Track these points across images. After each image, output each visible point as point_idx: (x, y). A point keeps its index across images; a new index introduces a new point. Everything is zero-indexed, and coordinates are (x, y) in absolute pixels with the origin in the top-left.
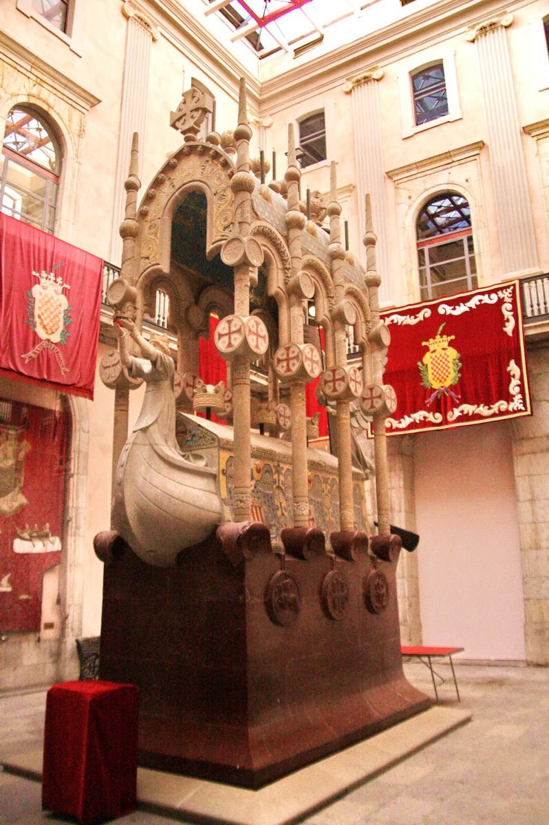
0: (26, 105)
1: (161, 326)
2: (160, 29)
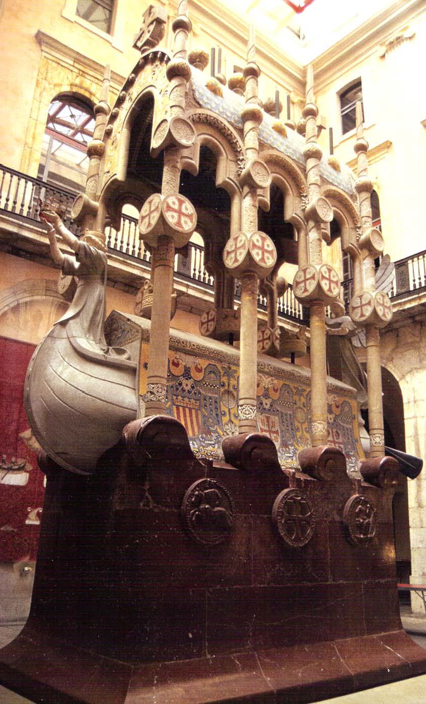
0: (69, 94)
1: (202, 281)
2: (200, 25)
